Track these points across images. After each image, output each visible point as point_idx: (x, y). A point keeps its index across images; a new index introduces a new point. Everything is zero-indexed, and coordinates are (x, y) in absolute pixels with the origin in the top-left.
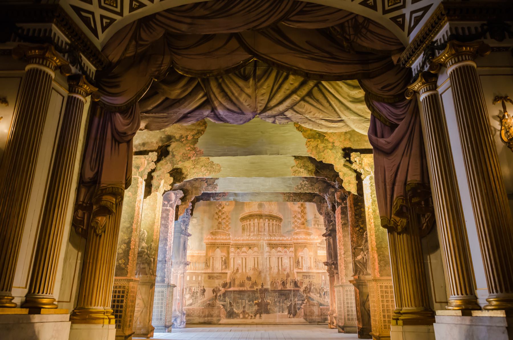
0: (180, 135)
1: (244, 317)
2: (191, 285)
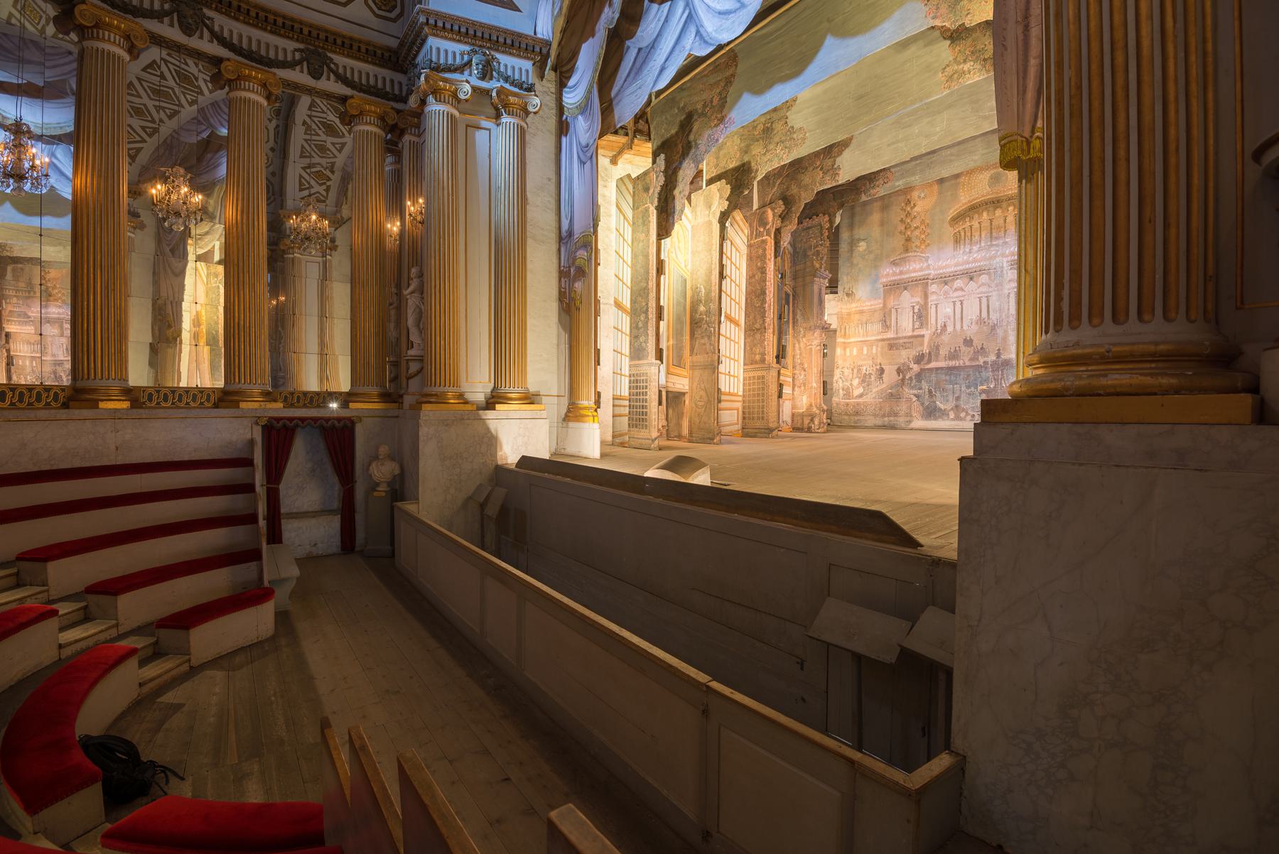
1: (958, 418)
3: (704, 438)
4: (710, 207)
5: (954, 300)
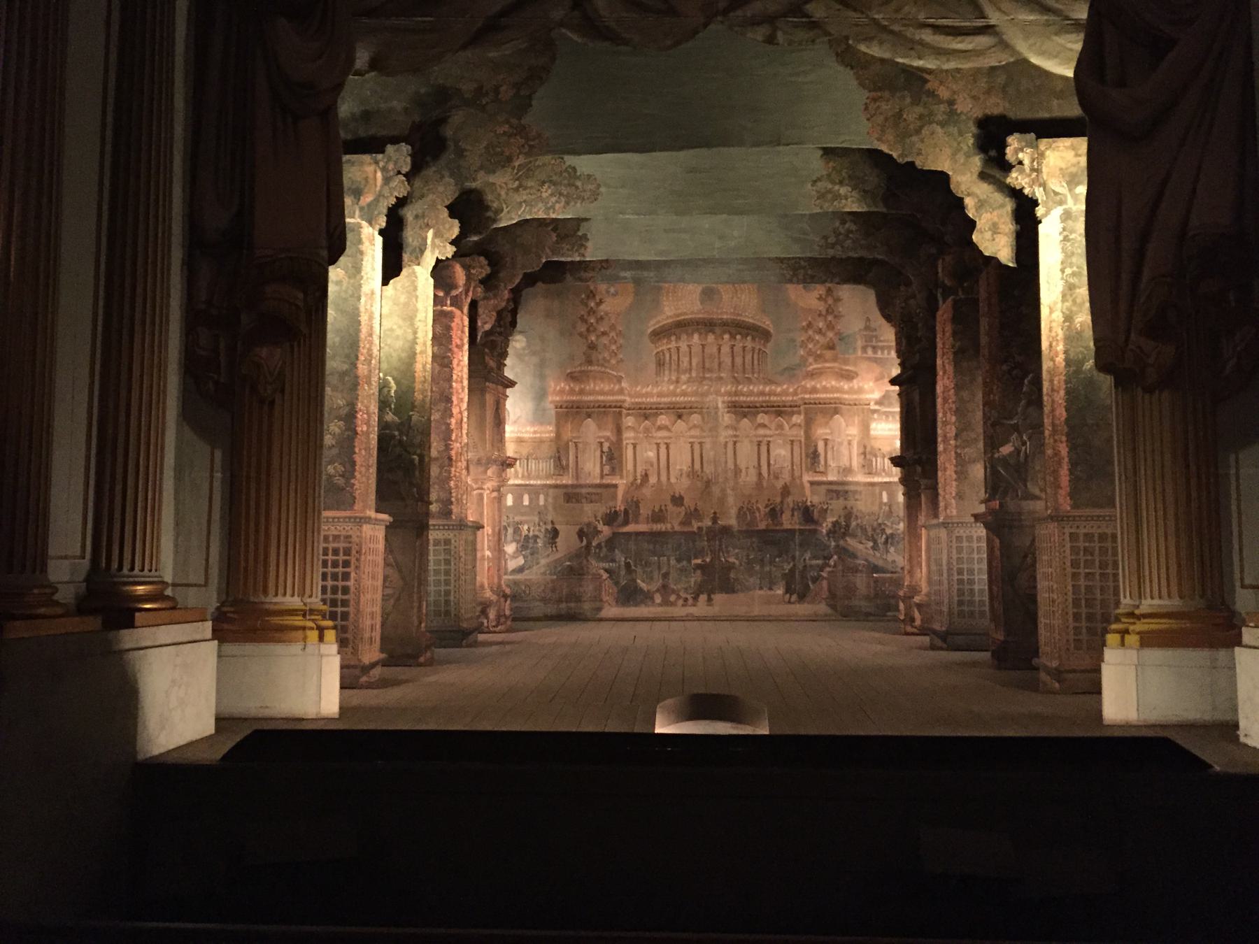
0: (476, 86)
1: (665, 603)
2: (517, 519)
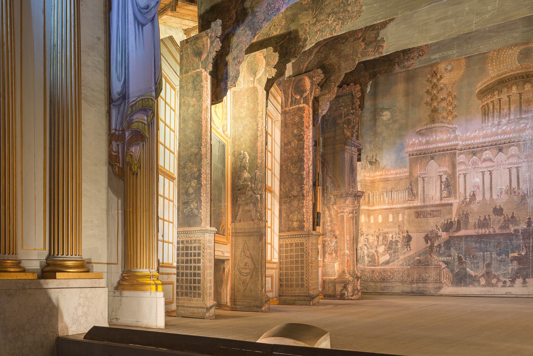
1: (489, 284)
2: (385, 230)
3: (250, 307)
4: (255, 74)
5: (483, 170)
